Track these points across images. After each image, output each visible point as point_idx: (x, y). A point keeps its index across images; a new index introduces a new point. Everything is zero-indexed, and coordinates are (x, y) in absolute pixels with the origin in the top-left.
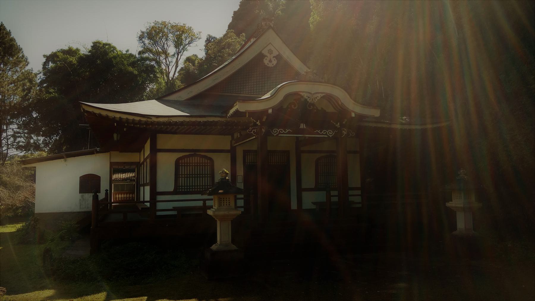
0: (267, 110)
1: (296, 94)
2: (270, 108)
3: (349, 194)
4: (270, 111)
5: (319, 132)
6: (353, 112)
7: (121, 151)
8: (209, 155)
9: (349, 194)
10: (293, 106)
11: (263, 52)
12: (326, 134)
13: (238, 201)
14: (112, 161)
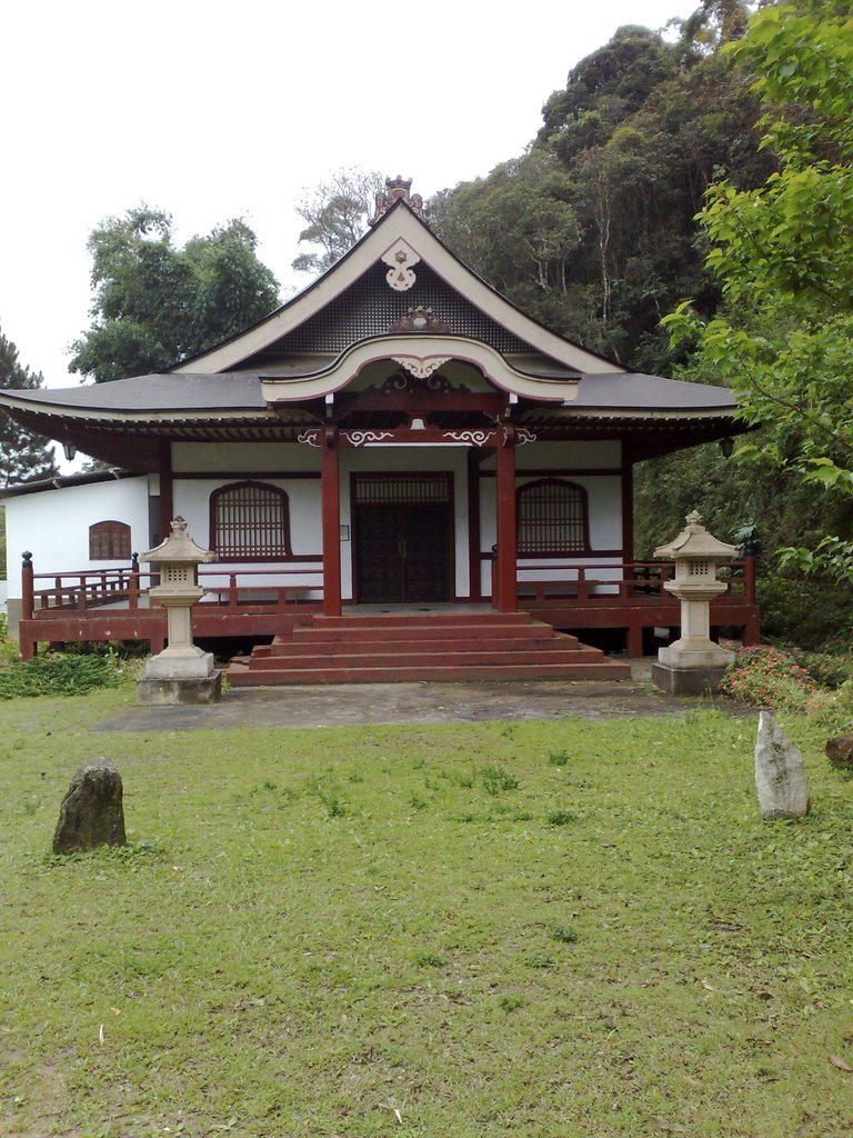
0: (322, 399)
1: (387, 361)
2: (328, 393)
4: (330, 399)
5: (453, 435)
6: (514, 393)
8: (277, 483)
11: (384, 259)
12: (470, 440)
13: (619, 547)
14: (152, 494)
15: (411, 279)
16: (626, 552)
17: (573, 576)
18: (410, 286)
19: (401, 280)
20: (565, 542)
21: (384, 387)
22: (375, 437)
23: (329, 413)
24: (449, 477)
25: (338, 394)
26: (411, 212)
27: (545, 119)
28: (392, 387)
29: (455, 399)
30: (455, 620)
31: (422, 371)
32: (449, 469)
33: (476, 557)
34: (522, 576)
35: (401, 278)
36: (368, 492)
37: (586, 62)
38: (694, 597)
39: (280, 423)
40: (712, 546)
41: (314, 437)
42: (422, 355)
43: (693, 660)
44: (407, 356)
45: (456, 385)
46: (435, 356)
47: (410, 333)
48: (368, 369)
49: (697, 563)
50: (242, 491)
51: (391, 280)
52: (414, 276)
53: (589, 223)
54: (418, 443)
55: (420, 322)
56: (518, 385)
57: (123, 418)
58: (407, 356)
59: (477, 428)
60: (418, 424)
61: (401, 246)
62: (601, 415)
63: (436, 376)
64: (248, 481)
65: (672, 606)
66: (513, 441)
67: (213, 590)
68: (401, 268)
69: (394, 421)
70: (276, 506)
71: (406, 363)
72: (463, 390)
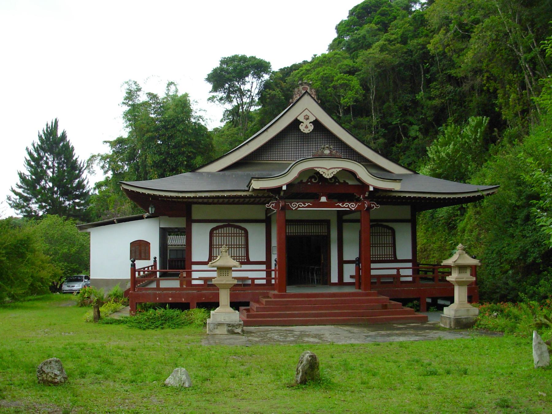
1: (312, 170)
2: (284, 185)
3: (265, 280)
4: (284, 188)
5: (340, 204)
6: (372, 185)
7: (170, 216)
9: (265, 280)
10: (313, 180)
11: (298, 118)
12: (348, 207)
13: (410, 257)
15: (311, 128)
16: (414, 261)
17: (394, 272)
18: (311, 130)
19: (306, 128)
20: (385, 255)
21: (308, 181)
22: (303, 205)
23: (282, 194)
24: (327, 223)
25: (288, 185)
26: (311, 96)
27: (338, 32)
28: (311, 182)
29: (343, 188)
30: (334, 295)
31: (328, 175)
32: (328, 218)
33: (341, 262)
34: (373, 272)
35: (307, 127)
36: (293, 230)
37: (356, 7)
38: (460, 283)
39: (257, 197)
40: (469, 261)
41: (274, 205)
42: (329, 167)
43: (463, 314)
44: (321, 168)
45: (342, 181)
46: (335, 168)
47: (321, 157)
48: (303, 173)
49: (462, 268)
50: (220, 230)
51: (302, 127)
52: (313, 126)
53: (364, 85)
54: (324, 208)
55: (327, 152)
56: (373, 182)
57: (181, 195)
58: (321, 168)
59: (352, 201)
60: (323, 199)
61: (306, 112)
62: (407, 195)
63: (334, 177)
64: (229, 223)
65: (450, 287)
66: (369, 208)
67: (200, 279)
68: (307, 123)
69: (314, 197)
70: (242, 236)
71: (321, 171)
72: (345, 183)
